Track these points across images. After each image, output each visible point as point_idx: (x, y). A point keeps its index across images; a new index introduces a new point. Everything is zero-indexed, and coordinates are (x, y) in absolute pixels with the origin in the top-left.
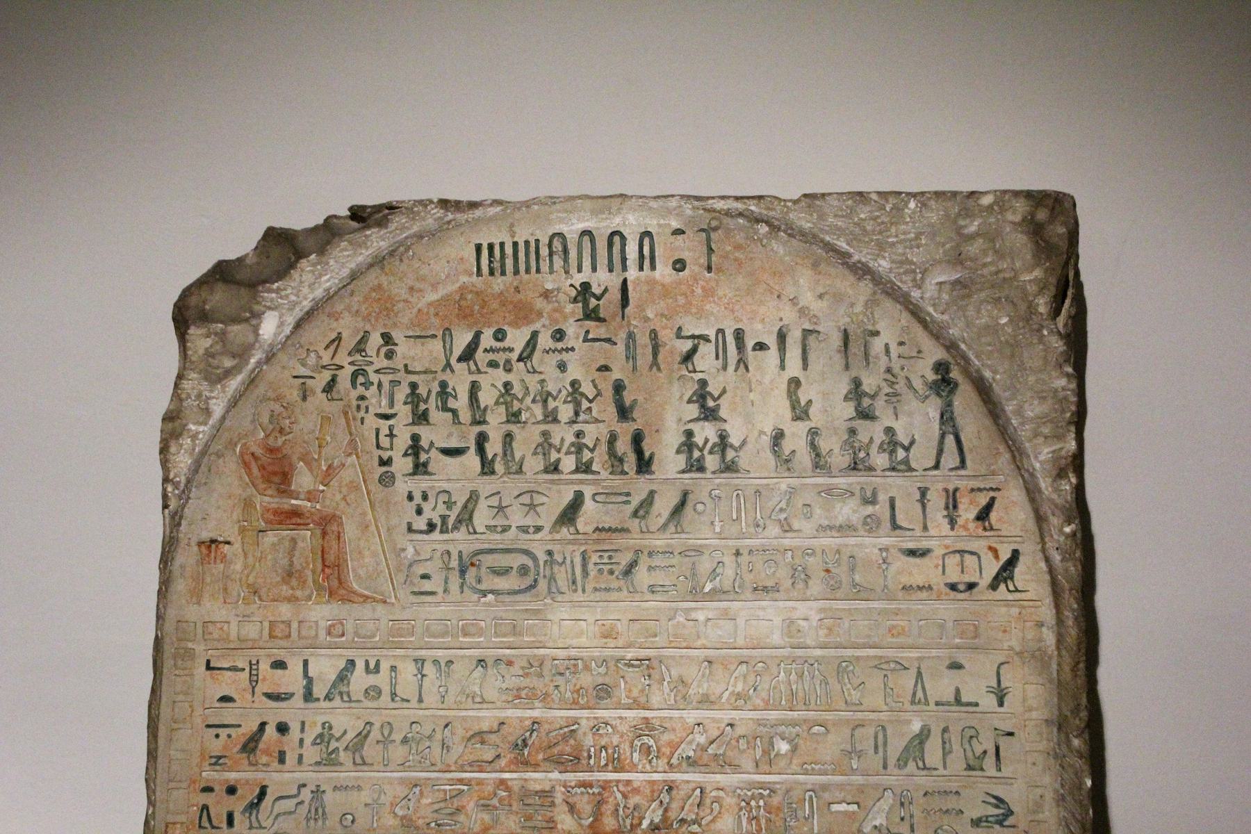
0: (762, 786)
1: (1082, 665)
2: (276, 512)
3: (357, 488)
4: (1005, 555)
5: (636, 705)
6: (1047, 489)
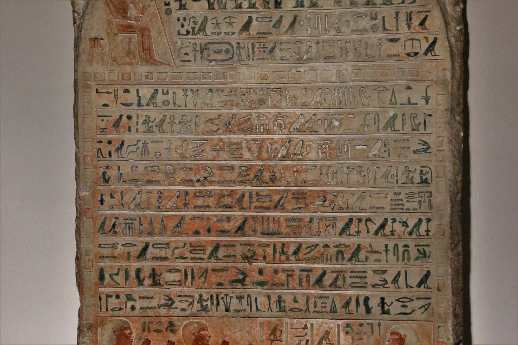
0: (328, 139)
1: (461, 86)
2: (122, 26)
3: (156, 15)
4: (431, 40)
5: (275, 107)
6: (450, 11)
